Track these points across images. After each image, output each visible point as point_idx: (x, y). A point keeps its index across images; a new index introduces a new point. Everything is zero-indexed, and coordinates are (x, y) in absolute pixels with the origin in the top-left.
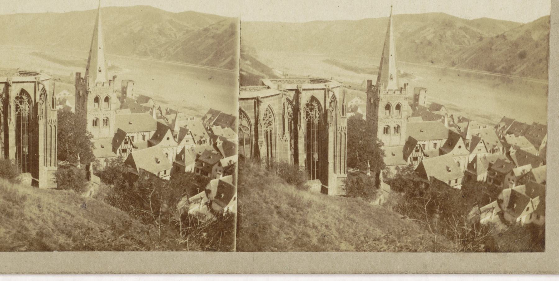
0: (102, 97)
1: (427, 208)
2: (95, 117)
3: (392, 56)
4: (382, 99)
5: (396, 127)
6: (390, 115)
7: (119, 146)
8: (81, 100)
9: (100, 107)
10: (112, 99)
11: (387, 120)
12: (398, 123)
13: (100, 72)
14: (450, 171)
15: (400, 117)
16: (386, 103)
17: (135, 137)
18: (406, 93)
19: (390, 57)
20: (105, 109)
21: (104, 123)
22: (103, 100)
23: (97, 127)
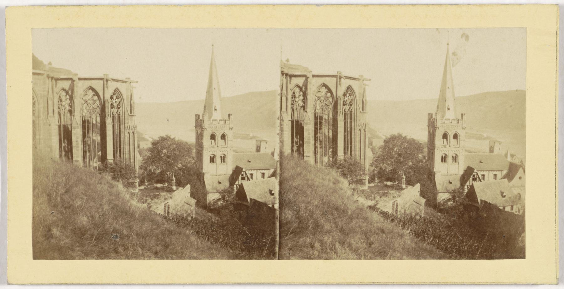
0: (217, 134)
1: (458, 236)
2: (212, 153)
3: (215, 89)
4: (438, 128)
5: (454, 156)
6: (447, 144)
7: (466, 182)
8: (432, 136)
9: (448, 143)
10: (228, 136)
11: (445, 149)
12: (445, 152)
13: (216, 111)
14: (504, 196)
15: (458, 146)
16: (211, 133)
17: (254, 175)
18: (463, 123)
19: (448, 90)
20: (454, 145)
21: (453, 160)
22: (220, 138)
23: (446, 164)
